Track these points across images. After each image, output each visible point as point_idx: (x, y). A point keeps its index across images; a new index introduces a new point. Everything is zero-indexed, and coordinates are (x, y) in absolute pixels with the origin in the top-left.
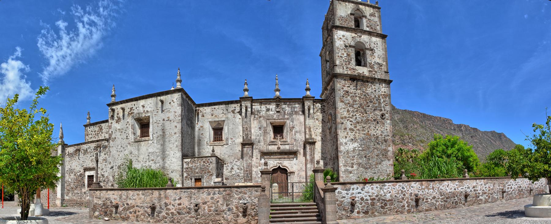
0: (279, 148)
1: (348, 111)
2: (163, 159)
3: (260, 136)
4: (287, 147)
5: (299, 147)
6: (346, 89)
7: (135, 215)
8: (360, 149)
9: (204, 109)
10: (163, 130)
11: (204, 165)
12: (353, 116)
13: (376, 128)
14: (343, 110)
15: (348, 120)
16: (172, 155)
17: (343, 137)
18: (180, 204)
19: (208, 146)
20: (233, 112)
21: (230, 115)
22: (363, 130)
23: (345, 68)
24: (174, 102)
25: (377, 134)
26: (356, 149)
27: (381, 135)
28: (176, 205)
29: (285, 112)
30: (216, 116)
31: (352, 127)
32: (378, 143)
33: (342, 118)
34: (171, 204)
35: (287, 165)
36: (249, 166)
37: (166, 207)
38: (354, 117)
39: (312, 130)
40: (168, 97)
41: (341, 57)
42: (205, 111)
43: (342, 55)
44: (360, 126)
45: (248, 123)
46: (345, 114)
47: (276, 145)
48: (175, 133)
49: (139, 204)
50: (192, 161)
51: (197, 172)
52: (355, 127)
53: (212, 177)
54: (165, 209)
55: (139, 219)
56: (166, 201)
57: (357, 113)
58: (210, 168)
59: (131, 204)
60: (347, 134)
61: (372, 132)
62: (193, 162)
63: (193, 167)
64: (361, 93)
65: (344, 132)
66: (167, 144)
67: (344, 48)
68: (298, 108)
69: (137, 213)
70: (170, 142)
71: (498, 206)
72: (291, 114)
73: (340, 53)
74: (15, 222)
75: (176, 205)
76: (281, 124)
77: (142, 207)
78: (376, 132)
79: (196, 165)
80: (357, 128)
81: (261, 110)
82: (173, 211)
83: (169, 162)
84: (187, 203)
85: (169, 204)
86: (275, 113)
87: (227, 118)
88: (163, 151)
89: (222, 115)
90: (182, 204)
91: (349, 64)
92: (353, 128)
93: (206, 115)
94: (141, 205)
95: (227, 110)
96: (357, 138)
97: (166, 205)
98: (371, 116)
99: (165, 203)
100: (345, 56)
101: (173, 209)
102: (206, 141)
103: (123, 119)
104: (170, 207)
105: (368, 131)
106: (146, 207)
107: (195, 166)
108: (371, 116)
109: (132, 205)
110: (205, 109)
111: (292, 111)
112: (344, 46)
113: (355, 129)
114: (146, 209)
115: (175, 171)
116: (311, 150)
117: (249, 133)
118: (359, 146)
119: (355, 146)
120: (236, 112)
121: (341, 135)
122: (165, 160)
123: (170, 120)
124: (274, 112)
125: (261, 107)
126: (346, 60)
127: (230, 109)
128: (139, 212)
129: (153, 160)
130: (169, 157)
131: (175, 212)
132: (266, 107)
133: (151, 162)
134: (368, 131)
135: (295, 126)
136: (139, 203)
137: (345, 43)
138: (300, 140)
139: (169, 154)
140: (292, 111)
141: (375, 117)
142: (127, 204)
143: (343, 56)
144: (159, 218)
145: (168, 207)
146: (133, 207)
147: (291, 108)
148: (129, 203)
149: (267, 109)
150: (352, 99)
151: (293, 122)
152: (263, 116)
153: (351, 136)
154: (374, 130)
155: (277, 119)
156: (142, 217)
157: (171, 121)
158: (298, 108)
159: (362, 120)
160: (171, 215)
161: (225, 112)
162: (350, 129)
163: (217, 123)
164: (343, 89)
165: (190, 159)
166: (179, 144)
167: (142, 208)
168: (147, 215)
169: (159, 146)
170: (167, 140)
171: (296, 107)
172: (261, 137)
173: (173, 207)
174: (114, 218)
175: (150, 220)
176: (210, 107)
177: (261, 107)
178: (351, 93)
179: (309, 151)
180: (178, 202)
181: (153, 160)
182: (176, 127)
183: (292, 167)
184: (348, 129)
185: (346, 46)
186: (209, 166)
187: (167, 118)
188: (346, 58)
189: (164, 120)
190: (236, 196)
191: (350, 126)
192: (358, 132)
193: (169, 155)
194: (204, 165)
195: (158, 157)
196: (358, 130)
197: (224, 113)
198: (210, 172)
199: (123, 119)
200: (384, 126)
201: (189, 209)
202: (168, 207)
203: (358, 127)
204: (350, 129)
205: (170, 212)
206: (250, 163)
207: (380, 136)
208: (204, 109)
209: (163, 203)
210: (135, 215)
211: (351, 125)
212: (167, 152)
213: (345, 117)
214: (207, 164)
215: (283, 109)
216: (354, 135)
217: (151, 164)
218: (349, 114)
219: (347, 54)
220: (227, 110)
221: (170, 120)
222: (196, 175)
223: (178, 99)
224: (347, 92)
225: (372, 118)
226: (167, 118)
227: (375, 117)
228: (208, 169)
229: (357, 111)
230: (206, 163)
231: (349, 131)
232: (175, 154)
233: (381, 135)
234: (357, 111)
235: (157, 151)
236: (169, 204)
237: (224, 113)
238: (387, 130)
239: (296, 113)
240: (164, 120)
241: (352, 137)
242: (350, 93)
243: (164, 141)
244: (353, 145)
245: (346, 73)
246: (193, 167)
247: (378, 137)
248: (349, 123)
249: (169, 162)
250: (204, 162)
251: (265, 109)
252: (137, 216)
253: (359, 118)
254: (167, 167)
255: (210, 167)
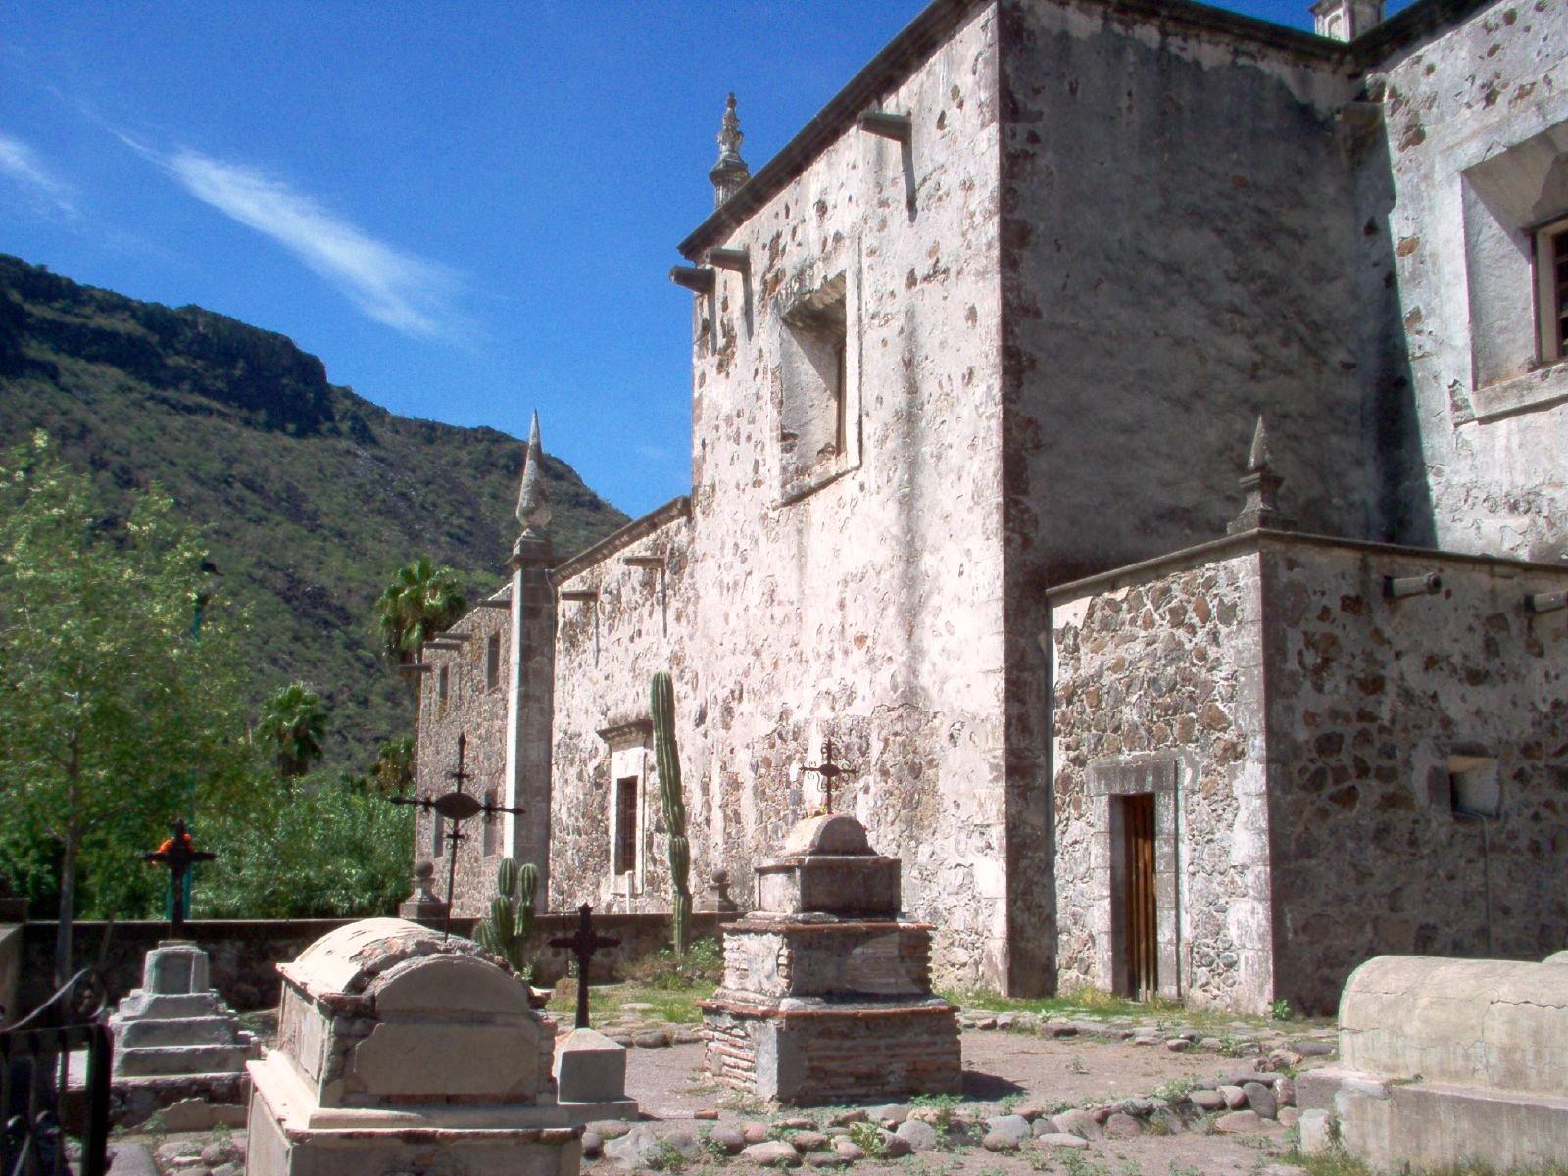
9: (1421, 68)
11: (1175, 652)
19: (1469, 430)
30: (1523, 93)
42: (1425, 86)
51: (1134, 727)
63: (1108, 679)
71: (898, 1051)
74: (776, 1171)
93: (1440, 118)
102: (1447, 379)
103: (750, 333)
110: (1425, 62)
163: (1546, 160)
165: (1086, 601)
176: (1467, 28)
189: (912, 281)
194: (1175, 652)
199: (750, 333)
208: (1421, 68)
222: (1125, 757)
230: (1192, 630)
246: (1108, 679)
250: (1177, 618)
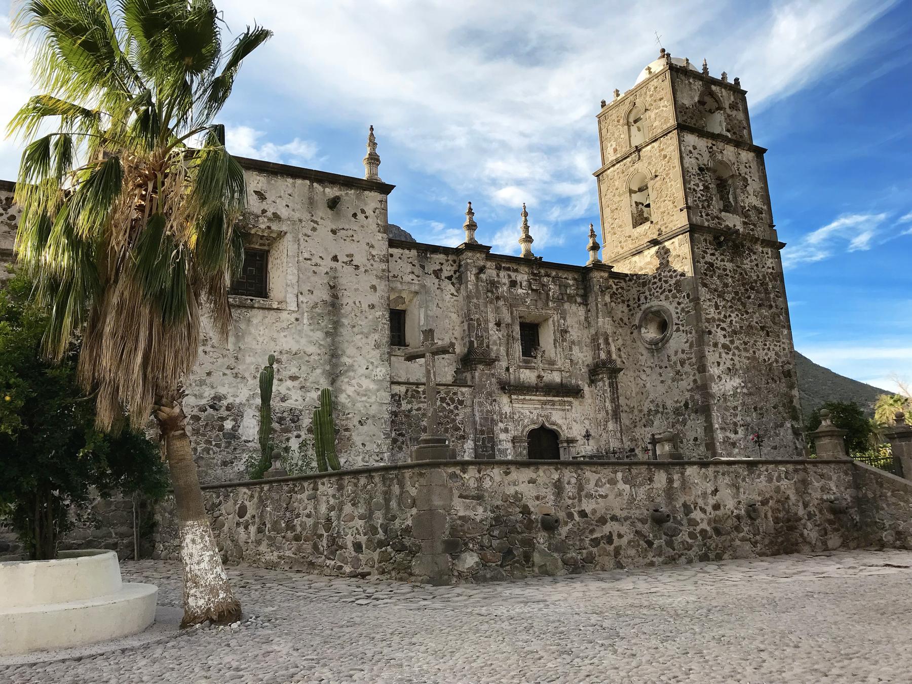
0: (539, 377)
1: (717, 307)
2: (334, 377)
3: (500, 346)
4: (556, 377)
5: (581, 380)
6: (708, 258)
7: (611, 548)
8: (745, 390)
10: (332, 287)
12: (725, 317)
13: (765, 345)
14: (708, 303)
15: (718, 326)
16: (362, 371)
17: (713, 363)
18: (716, 507)
20: (437, 274)
21: (431, 282)
22: (746, 350)
23: (704, 214)
24: (366, 217)
25: (769, 359)
26: (739, 391)
27: (777, 361)
28: (709, 509)
29: (548, 295)
31: (727, 341)
32: (773, 379)
33: (708, 320)
34: (698, 508)
35: (560, 422)
36: (486, 419)
37: (687, 515)
38: (728, 320)
39: (610, 340)
40: (347, 194)
41: (694, 190)
43: (696, 188)
44: (740, 340)
45: (482, 309)
46: (712, 312)
47: (534, 368)
48: (372, 307)
49: (618, 513)
50: (410, 393)
52: (732, 342)
53: (463, 443)
54: (685, 522)
55: (624, 561)
56: (687, 498)
57: (732, 312)
58: (459, 418)
59: (594, 511)
60: (720, 357)
61: (761, 354)
62: (413, 396)
64: (734, 270)
65: (714, 351)
66: (345, 332)
67: (699, 172)
68: (573, 288)
69: (616, 541)
70: (356, 330)
72: (560, 300)
73: (692, 183)
75: (709, 509)
76: (536, 322)
77: (626, 518)
78: (766, 354)
79: (421, 405)
80: (735, 345)
81: (498, 282)
82: (704, 526)
83: (353, 389)
84: (732, 502)
85: (692, 506)
86: (528, 294)
87: (424, 286)
88: (334, 354)
89: (411, 276)
90: (722, 508)
91: (709, 206)
92: (728, 343)
94: (625, 514)
95: (423, 267)
96: (738, 367)
97: (687, 509)
98: (755, 320)
99: (685, 505)
100: (701, 190)
101: (702, 520)
104: (697, 515)
105: (754, 352)
106: (639, 520)
107: (419, 409)
108: (755, 320)
109: (598, 515)
111: (562, 294)
112: (697, 168)
113: (732, 346)
114: (639, 525)
115: (369, 421)
116: (613, 388)
117: (485, 334)
118: (743, 384)
119: (735, 385)
120: (443, 278)
121: (709, 358)
122: (338, 383)
123: (354, 263)
124: (524, 291)
125: (498, 275)
126: (704, 198)
127: (432, 267)
128: (620, 536)
129: (293, 378)
130: (351, 374)
131: (708, 529)
132: (510, 276)
133: (289, 383)
134: (754, 352)
135: (570, 329)
136: (616, 506)
137: (699, 162)
138: (580, 362)
139: (352, 366)
140: (562, 294)
141: (763, 320)
142: (583, 514)
143: (698, 190)
144: (674, 550)
145: (693, 515)
146: (602, 521)
147: (560, 286)
148: (588, 510)
149: (511, 281)
150: (721, 282)
151: (565, 319)
152: (504, 297)
153: (727, 363)
154: (764, 349)
155: (530, 309)
156: (632, 552)
157: (357, 267)
158: (573, 288)
159: (741, 327)
160: (700, 538)
161: (417, 270)
162: (725, 346)
164: (703, 258)
166: (384, 341)
167: (628, 522)
168: (645, 545)
169: (319, 335)
170: (345, 321)
171: (570, 286)
172: (502, 348)
173: (703, 516)
174: (541, 567)
175: (654, 559)
177: (498, 275)
178: (719, 269)
179: (608, 390)
180: (712, 501)
181: (293, 378)
182: (374, 288)
183: (571, 428)
184: (720, 346)
185: (701, 169)
186: (456, 412)
187: (347, 256)
188: (702, 192)
190: (816, 484)
191: (722, 340)
192: (736, 352)
193: (351, 368)
195: (314, 369)
196: (737, 348)
197: (416, 272)
198: (457, 429)
200: (779, 342)
201: (738, 517)
202: (693, 515)
203: (737, 343)
204: (725, 346)
205: (698, 528)
206: (488, 411)
207: (775, 364)
209: (679, 504)
210: (611, 548)
211: (725, 336)
212: (345, 360)
213: (714, 319)
214: (452, 407)
215: (544, 285)
216: (732, 359)
217: (289, 389)
218: (719, 313)
219: (703, 185)
220: (423, 267)
221: (354, 263)
223: (377, 211)
224: (711, 265)
225: (757, 323)
226: (347, 256)
227: (763, 320)
228: (454, 420)
229: (731, 307)
231: (722, 350)
232: (371, 367)
233: (777, 361)
234: (731, 307)
235: (311, 349)
236: (692, 506)
237: (416, 272)
238: (784, 349)
239: (571, 299)
240: (335, 259)
241: (729, 364)
242: (717, 267)
243: (337, 324)
244: (732, 383)
245: (706, 224)
246: (414, 412)
247: (771, 364)
248: (720, 333)
249: (353, 389)
251: (506, 280)
252: (617, 551)
253: (736, 322)
254: (343, 406)
255: (457, 414)
